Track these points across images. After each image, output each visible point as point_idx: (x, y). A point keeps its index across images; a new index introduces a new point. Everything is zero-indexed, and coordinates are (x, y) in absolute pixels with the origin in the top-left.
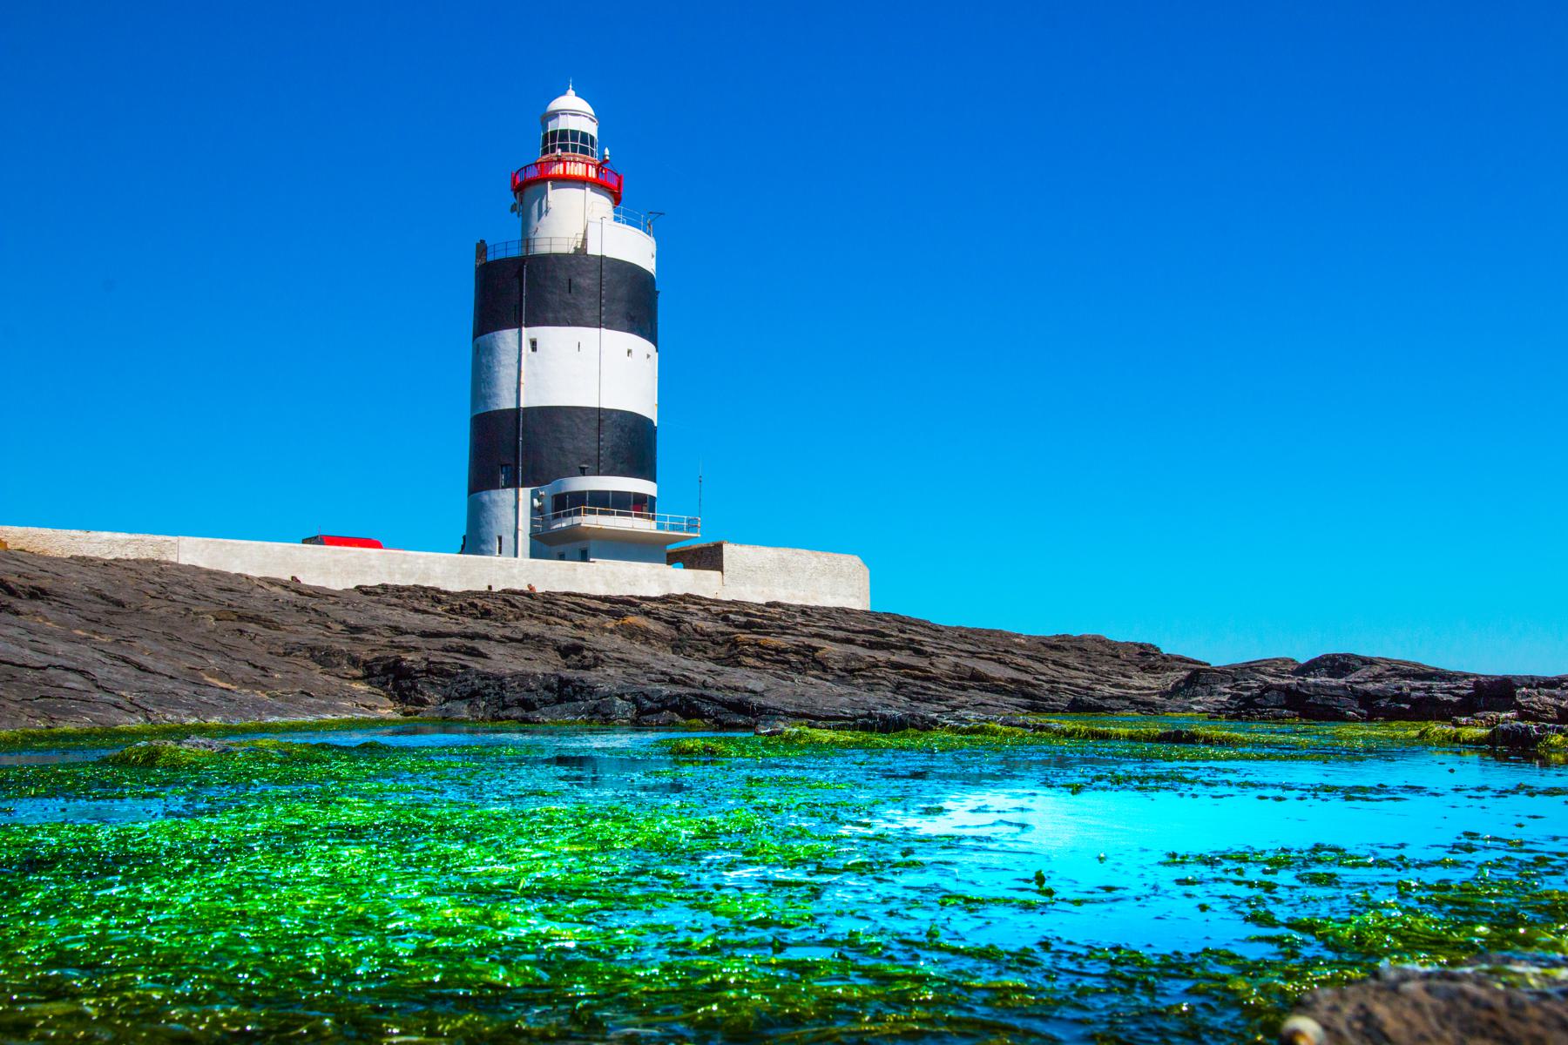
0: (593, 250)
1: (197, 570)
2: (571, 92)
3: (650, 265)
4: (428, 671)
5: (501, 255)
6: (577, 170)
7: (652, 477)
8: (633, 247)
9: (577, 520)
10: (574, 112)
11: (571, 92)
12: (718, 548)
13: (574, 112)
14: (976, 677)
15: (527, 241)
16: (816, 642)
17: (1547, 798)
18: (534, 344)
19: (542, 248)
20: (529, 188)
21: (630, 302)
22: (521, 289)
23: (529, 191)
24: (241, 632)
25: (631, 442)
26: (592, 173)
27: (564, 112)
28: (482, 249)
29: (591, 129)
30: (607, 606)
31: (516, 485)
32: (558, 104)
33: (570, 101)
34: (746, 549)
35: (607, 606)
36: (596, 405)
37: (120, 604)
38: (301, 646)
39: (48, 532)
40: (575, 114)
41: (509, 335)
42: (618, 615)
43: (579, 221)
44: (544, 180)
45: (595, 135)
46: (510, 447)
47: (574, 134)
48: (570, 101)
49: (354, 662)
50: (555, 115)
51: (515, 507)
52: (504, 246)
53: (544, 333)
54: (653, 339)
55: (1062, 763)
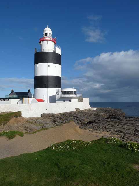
2: (48, 27)
11: (48, 27)
13: (48, 30)
21: (57, 59)
22: (41, 57)
32: (46, 29)
43: (48, 46)
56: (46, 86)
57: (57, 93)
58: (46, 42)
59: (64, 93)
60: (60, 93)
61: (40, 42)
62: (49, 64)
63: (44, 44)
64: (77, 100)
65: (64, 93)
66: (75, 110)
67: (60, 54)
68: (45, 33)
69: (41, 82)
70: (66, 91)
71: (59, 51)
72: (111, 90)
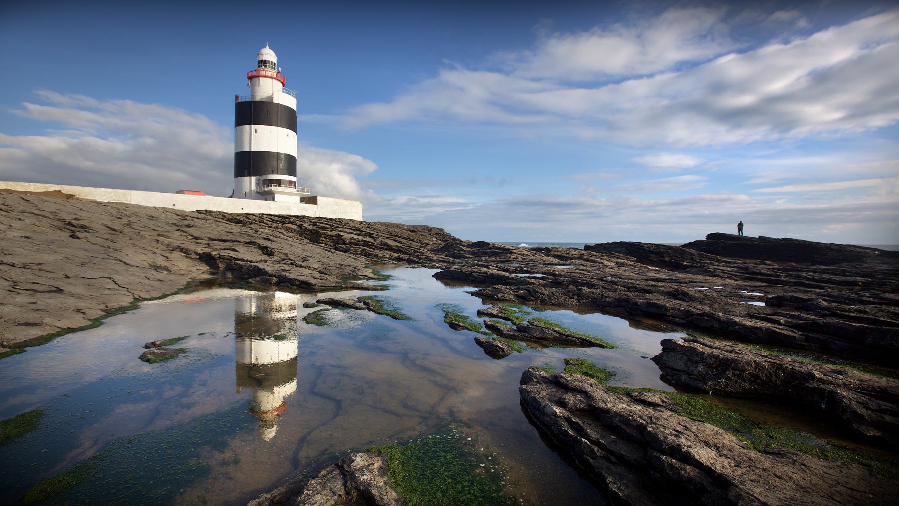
0: (275, 101)
1: (140, 207)
3: (294, 107)
4: (220, 258)
5: (244, 100)
6: (269, 74)
7: (295, 175)
8: (290, 102)
9: (270, 188)
10: (269, 55)
12: (316, 197)
13: (269, 55)
14: (386, 244)
15: (253, 96)
16: (342, 234)
19: (258, 99)
21: (289, 119)
22: (251, 112)
23: (255, 80)
24: (158, 241)
25: (290, 165)
26: (275, 76)
28: (237, 97)
30: (279, 219)
31: (250, 176)
35: (279, 219)
37: (114, 230)
38: (178, 247)
39: (80, 188)
41: (247, 127)
42: (283, 223)
43: (270, 89)
44: (258, 77)
46: (250, 163)
49: (196, 253)
51: (251, 183)
52: (245, 97)
54: (295, 132)
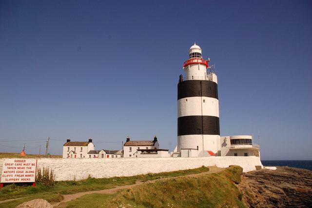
2: (195, 44)
10: (196, 49)
11: (195, 44)
13: (196, 49)
17: (57, 154)
18: (187, 100)
20: (188, 64)
21: (211, 90)
22: (187, 89)
27: (193, 49)
29: (200, 52)
32: (193, 47)
33: (195, 46)
34: (206, 113)
36: (200, 114)
40: (196, 49)
43: (198, 73)
45: (201, 53)
47: (196, 53)
48: (195, 46)
50: (191, 50)
53: (187, 98)
55: (207, 185)
56: (201, 132)
57: (224, 144)
58: (196, 67)
59: (234, 142)
60: (228, 142)
61: (186, 66)
62: (204, 98)
63: (203, 68)
64: (58, 180)
65: (234, 142)
66: (255, 169)
67: (217, 82)
68: (193, 53)
69: (189, 126)
70: (238, 140)
71: (215, 79)
72: (69, 167)
